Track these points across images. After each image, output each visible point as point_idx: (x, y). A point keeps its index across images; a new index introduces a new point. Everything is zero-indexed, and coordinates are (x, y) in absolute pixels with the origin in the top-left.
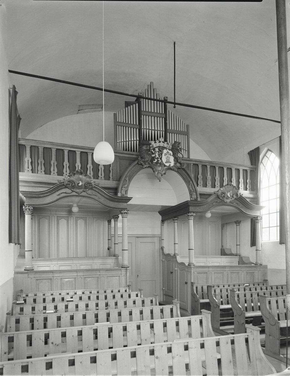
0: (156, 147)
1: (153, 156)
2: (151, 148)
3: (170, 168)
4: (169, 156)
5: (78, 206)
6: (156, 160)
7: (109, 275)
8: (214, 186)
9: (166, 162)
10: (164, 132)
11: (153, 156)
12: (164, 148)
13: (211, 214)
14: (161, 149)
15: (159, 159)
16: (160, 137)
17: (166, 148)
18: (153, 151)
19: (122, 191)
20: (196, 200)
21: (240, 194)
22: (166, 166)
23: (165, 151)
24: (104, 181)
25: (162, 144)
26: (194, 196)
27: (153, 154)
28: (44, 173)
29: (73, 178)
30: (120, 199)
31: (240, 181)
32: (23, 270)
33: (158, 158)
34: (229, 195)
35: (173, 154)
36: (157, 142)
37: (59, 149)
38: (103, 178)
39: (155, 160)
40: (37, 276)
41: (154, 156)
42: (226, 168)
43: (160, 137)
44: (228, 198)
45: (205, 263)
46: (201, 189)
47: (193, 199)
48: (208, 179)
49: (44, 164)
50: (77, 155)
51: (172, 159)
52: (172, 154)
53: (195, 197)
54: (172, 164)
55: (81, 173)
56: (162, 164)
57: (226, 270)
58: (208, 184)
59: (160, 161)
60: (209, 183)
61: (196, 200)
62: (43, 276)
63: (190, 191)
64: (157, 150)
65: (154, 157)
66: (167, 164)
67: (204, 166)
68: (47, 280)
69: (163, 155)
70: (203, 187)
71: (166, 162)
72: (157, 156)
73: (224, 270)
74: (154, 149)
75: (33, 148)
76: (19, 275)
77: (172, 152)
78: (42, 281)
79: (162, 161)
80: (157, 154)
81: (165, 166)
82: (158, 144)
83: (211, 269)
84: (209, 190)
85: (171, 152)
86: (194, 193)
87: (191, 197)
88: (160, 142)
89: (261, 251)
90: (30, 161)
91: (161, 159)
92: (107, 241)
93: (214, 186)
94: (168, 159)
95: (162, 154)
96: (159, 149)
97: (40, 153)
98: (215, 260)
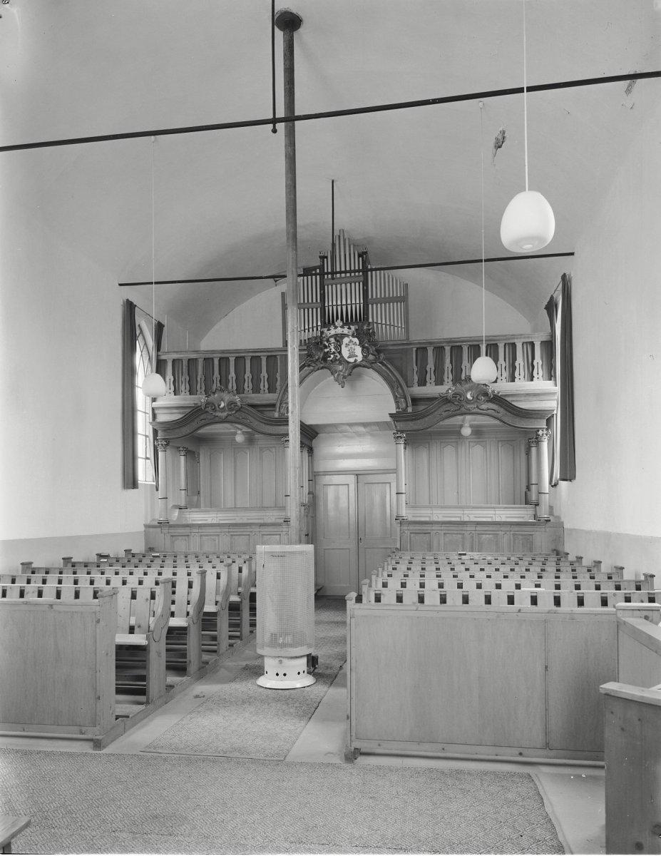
0: (331, 337)
1: (326, 350)
2: (325, 339)
3: (356, 366)
4: (353, 346)
5: (471, 426)
6: (332, 356)
7: (264, 533)
8: (256, 390)
9: (349, 357)
10: (362, 305)
11: (326, 350)
12: (343, 336)
13: (460, 431)
14: (339, 338)
15: (337, 354)
16: (337, 318)
17: (347, 336)
18: (326, 343)
19: (282, 410)
20: (405, 410)
21: (493, 391)
22: (350, 363)
23: (346, 340)
24: (268, 395)
25: (339, 330)
26: (401, 403)
27: (326, 347)
28: (188, 393)
29: (212, 398)
30: (280, 421)
31: (517, 364)
32: (156, 523)
33: (334, 353)
34: (469, 396)
35: (360, 343)
36: (332, 328)
37: (271, 356)
38: (267, 391)
39: (330, 357)
40: (172, 531)
41: (328, 350)
42: (433, 348)
43: (337, 318)
44: (468, 401)
45: (461, 517)
46: (418, 391)
47: (400, 410)
48: (446, 369)
49: (189, 381)
50: (231, 363)
51: (358, 350)
52: (358, 343)
53: (404, 405)
54: (360, 358)
55: (222, 391)
56: (342, 361)
57: (468, 529)
58: (446, 379)
59: (339, 356)
60: (264, 385)
61: (405, 410)
62: (179, 531)
63: (395, 397)
64: (332, 340)
65: (328, 352)
66: (352, 360)
67: (439, 350)
68: (184, 538)
69: (343, 346)
70: (436, 385)
71: (349, 357)
72: (333, 350)
73: (465, 528)
74: (328, 341)
75: (191, 362)
76: (151, 530)
77: (358, 339)
78: (177, 537)
79: (342, 357)
80: (332, 347)
81: (348, 363)
82: (333, 332)
83: (436, 527)
84: (431, 390)
85: (356, 340)
86: (402, 400)
87: (398, 407)
88: (336, 327)
89: (404, 495)
90: (172, 379)
91: (340, 353)
92: (307, 481)
93: (240, 390)
94: (352, 350)
95: (340, 346)
96: (335, 339)
97: (184, 367)
98: (485, 512)
